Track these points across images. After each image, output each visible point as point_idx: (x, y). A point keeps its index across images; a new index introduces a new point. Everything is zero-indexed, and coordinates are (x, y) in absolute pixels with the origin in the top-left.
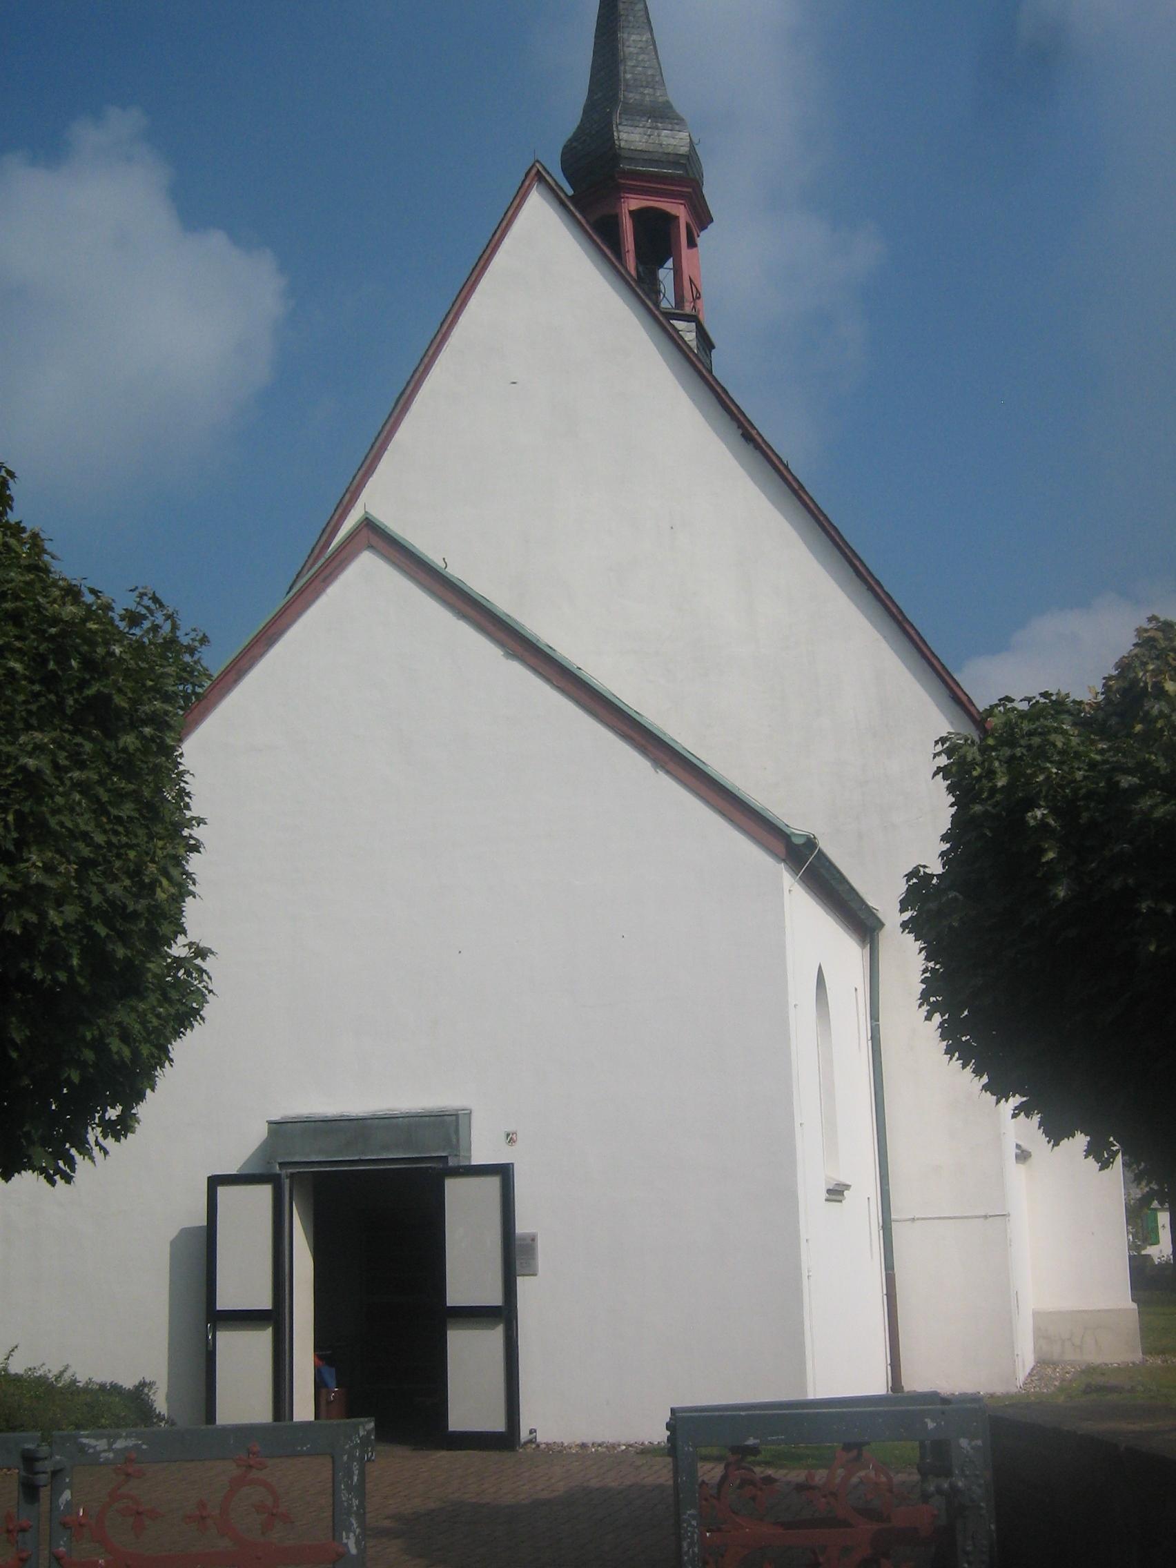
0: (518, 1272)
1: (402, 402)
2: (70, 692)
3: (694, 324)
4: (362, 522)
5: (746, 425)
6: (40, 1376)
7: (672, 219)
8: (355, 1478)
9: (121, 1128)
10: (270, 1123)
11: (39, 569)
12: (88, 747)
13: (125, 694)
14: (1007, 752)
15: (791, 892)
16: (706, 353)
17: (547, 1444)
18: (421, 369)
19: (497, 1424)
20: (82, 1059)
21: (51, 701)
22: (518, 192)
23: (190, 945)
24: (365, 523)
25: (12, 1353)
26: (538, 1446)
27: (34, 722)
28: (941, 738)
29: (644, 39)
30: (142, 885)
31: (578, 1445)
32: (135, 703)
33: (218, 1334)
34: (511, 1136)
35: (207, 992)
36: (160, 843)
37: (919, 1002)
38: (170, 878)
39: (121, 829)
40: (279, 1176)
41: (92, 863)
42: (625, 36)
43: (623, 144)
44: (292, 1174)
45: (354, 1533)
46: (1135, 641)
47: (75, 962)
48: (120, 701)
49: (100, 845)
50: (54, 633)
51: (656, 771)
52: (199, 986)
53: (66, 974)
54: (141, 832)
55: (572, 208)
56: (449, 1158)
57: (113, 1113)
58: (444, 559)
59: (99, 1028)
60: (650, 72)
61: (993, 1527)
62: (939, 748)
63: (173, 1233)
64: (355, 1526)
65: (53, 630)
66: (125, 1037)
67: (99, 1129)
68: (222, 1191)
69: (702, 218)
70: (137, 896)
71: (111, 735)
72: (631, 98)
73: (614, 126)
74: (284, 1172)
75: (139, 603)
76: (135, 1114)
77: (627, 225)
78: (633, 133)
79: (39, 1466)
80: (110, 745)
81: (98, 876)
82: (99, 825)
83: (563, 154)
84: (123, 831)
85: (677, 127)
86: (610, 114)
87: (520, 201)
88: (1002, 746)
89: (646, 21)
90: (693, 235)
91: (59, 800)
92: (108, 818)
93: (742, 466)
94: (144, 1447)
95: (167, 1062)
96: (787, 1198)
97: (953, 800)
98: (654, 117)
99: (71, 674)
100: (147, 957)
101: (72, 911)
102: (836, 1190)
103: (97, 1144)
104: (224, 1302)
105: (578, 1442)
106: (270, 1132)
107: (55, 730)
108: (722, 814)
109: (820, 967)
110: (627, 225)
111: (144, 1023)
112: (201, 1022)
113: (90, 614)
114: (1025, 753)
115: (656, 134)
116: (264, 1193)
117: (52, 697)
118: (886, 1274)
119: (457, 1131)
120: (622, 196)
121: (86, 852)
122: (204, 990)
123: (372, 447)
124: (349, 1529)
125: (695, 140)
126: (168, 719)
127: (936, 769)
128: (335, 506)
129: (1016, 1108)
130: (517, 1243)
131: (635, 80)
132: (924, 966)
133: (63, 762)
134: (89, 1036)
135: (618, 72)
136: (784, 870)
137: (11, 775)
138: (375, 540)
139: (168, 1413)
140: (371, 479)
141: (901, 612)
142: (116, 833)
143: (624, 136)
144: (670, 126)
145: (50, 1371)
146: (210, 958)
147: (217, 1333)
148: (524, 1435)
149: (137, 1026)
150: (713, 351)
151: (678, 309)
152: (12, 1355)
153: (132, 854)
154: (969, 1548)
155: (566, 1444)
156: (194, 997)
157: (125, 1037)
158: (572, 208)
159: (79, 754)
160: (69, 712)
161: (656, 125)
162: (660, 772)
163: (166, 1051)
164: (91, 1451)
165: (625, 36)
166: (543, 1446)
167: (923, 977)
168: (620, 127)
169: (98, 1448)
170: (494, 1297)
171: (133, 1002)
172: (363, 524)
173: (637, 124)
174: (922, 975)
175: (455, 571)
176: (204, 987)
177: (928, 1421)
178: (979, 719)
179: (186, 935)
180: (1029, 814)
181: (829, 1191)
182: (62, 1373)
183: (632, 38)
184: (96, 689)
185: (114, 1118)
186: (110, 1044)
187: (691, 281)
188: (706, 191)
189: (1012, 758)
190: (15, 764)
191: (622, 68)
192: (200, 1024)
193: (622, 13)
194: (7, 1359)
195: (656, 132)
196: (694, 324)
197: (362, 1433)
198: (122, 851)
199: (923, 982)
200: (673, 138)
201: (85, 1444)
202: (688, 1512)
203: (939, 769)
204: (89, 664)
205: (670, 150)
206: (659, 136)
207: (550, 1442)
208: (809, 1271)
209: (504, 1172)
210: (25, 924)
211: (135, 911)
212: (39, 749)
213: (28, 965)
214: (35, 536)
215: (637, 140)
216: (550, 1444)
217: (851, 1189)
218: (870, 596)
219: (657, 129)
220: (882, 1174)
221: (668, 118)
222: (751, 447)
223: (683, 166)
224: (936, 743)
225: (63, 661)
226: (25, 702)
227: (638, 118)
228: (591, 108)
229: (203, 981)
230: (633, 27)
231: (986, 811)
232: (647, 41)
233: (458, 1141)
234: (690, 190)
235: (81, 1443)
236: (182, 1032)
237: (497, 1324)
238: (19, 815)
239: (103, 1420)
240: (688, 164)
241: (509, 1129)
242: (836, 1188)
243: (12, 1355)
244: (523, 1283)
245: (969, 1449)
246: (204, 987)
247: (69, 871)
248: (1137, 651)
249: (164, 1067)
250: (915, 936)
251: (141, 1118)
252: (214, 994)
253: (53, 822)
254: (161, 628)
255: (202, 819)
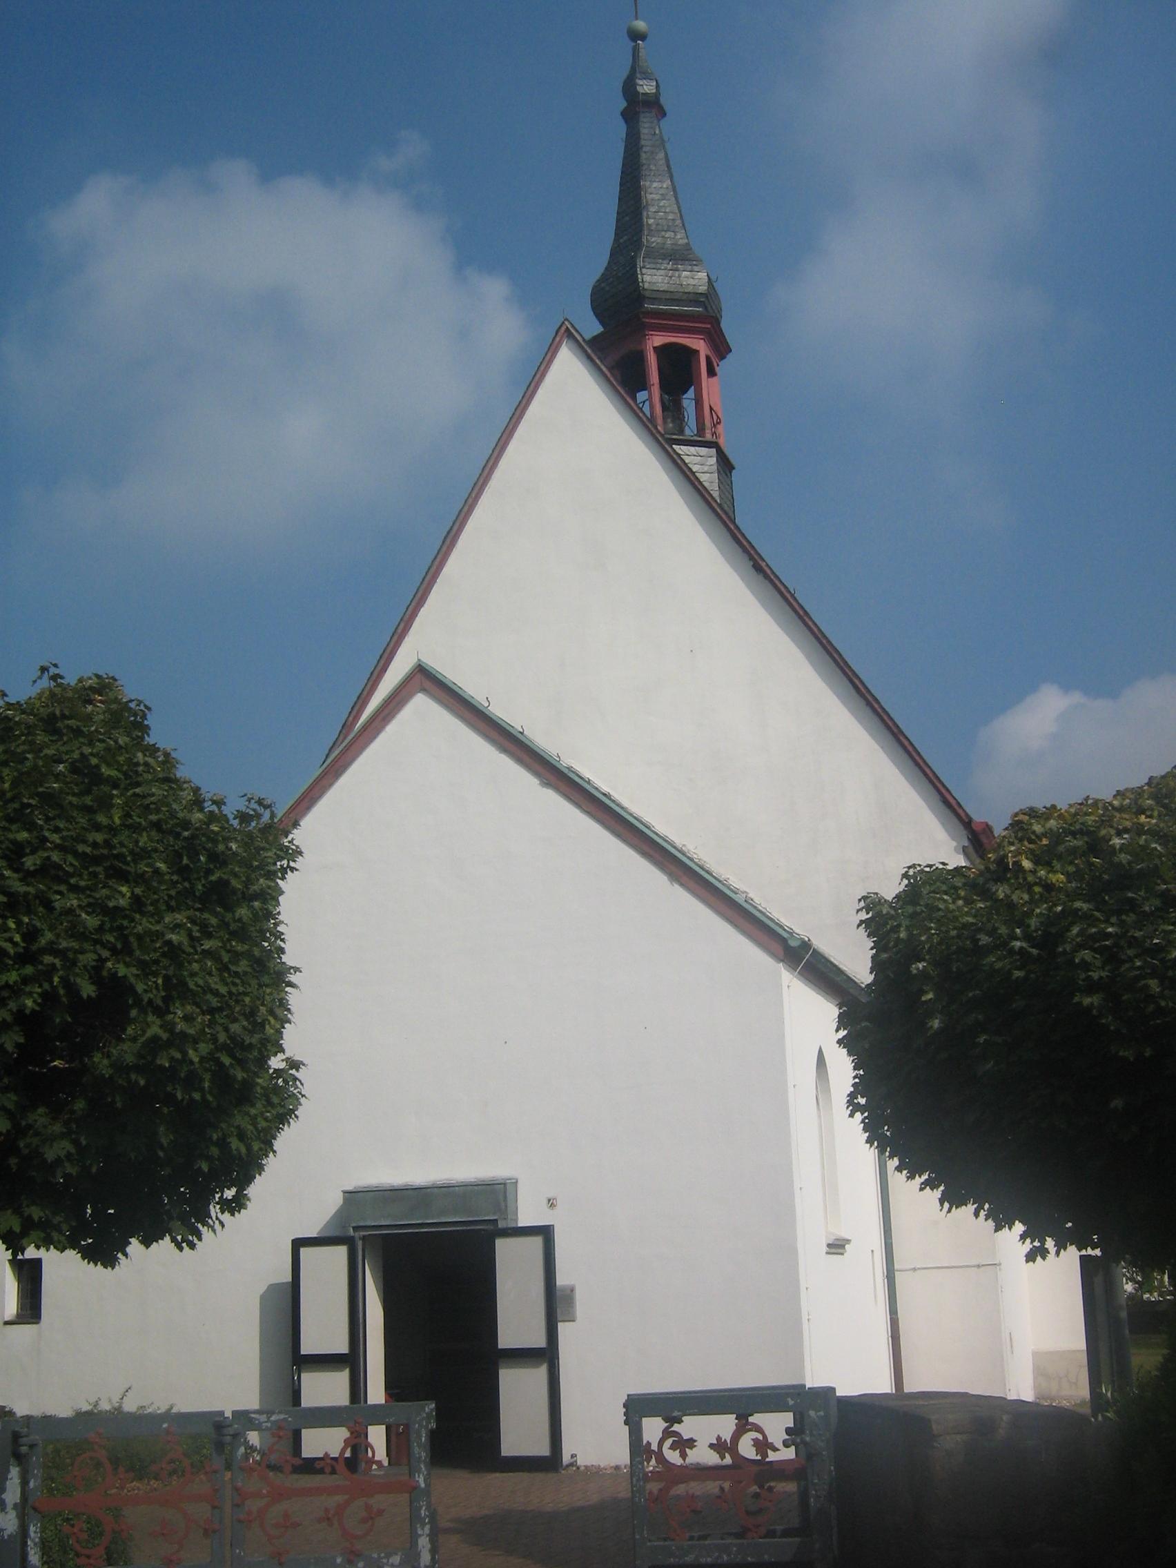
0: (559, 1319)
2: (199, 879)
3: (714, 450)
4: (416, 668)
8: (423, 1439)
9: (235, 1205)
10: (345, 1192)
11: (169, 780)
12: (214, 921)
13: (240, 877)
14: (910, 909)
16: (726, 475)
17: (586, 1467)
19: (544, 1450)
21: (186, 888)
23: (287, 1060)
25: (127, 1393)
26: (578, 1468)
27: (173, 903)
29: (665, 186)
30: (255, 1023)
31: (612, 1467)
32: (248, 882)
33: (303, 1375)
34: (551, 1201)
35: (300, 1096)
36: (268, 991)
37: (846, 1106)
38: (276, 1017)
39: (238, 981)
40: (353, 1237)
41: (220, 1009)
42: (648, 184)
43: (646, 286)
44: (364, 1236)
46: (1010, 822)
48: (235, 883)
51: (671, 883)
52: (295, 1091)
53: (199, 1094)
57: (230, 1193)
58: (487, 698)
59: (222, 1129)
61: (832, 1468)
62: (862, 904)
63: (262, 1288)
64: (423, 1469)
65: (186, 834)
66: (242, 1136)
67: (218, 1207)
68: (304, 1252)
69: (721, 348)
70: (251, 1032)
71: (229, 908)
72: (653, 242)
73: (638, 269)
77: (652, 360)
79: (226, 1431)
80: (229, 916)
82: (223, 980)
85: (696, 268)
86: (634, 259)
87: (547, 365)
90: (713, 366)
91: (196, 966)
92: (229, 974)
94: (290, 1419)
95: (271, 1153)
96: (787, 1253)
98: (674, 260)
100: (256, 1075)
101: (204, 1048)
102: (835, 1245)
103: (217, 1218)
104: (307, 1348)
105: (613, 1464)
106: (345, 1199)
109: (820, 1051)
110: (652, 360)
112: (296, 1119)
113: (212, 817)
114: (924, 909)
115: (677, 275)
116: (341, 1252)
117: (187, 884)
118: (891, 1319)
120: (647, 333)
121: (215, 1002)
122: (298, 1094)
123: (423, 580)
125: (713, 278)
129: (922, 1184)
130: (558, 1293)
131: (658, 225)
134: (215, 1137)
136: (783, 969)
137: (160, 948)
138: (428, 684)
142: (235, 984)
143: (647, 278)
146: (303, 1069)
147: (302, 1374)
148: (566, 1459)
150: (734, 471)
151: (700, 437)
152: (126, 1395)
153: (247, 1000)
154: (816, 1481)
155: (602, 1466)
157: (242, 1136)
162: (675, 884)
163: (271, 1145)
164: (257, 1422)
165: (648, 184)
167: (853, 1082)
168: (644, 271)
172: (417, 670)
174: (854, 1079)
175: (498, 710)
176: (298, 1092)
178: (967, 820)
179: (284, 1053)
180: (914, 966)
181: (829, 1246)
184: (218, 875)
185: (230, 1198)
187: (711, 409)
191: (645, 214)
192: (295, 1122)
193: (644, 162)
194: (122, 1398)
195: (677, 274)
196: (714, 450)
198: (240, 998)
200: (693, 278)
201: (253, 1418)
203: (862, 922)
204: (213, 857)
205: (690, 289)
206: (679, 276)
207: (589, 1464)
209: (546, 1233)
210: (172, 1059)
211: (251, 1044)
212: (177, 927)
214: (167, 755)
218: (868, 710)
220: (886, 1228)
222: (761, 577)
224: (860, 900)
229: (298, 1088)
230: (654, 175)
231: (890, 957)
232: (667, 188)
233: (506, 1206)
234: (709, 326)
235: (250, 1417)
236: (281, 1128)
237: (541, 1364)
238: (167, 979)
239: (205, 1451)
241: (550, 1196)
242: (835, 1243)
243: (126, 1395)
245: (815, 1417)
246: (298, 1092)
247: (205, 1021)
250: (848, 1050)
251: (251, 1197)
252: (306, 1098)
253: (192, 985)
254: (262, 815)
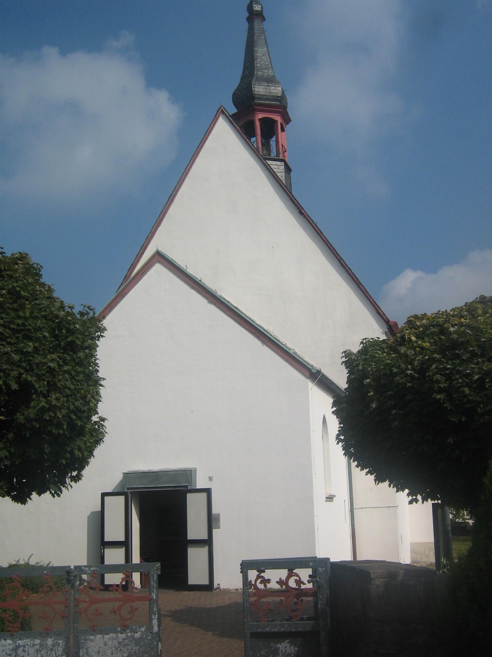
1: (171, 198)
2: (62, 340)
3: (283, 163)
5: (301, 208)
6: (41, 566)
7: (275, 122)
9: (77, 479)
10: (124, 473)
15: (312, 390)
18: (178, 186)
19: (206, 582)
20: (66, 457)
22: (214, 118)
23: (99, 417)
24: (157, 253)
25: (31, 557)
26: (221, 590)
27: (51, 350)
28: (344, 352)
30: (86, 402)
32: (83, 342)
35: (105, 433)
36: (92, 388)
37: (336, 439)
39: (79, 384)
41: (71, 395)
42: (257, 49)
44: (132, 492)
45: (155, 593)
47: (65, 427)
48: (78, 342)
49: (73, 389)
50: (57, 321)
54: (85, 384)
55: (235, 124)
56: (188, 486)
57: (74, 474)
59: (71, 446)
60: (267, 63)
61: (328, 592)
62: (343, 355)
63: (88, 514)
64: (155, 591)
66: (80, 449)
67: (70, 479)
69: (287, 120)
70: (84, 405)
71: (75, 352)
72: (259, 74)
73: (252, 85)
74: (129, 491)
75: (84, 310)
76: (81, 474)
77: (258, 124)
78: (260, 88)
79: (71, 574)
80: (75, 356)
81: (72, 399)
82: (72, 383)
83: (233, 96)
84: (79, 384)
85: (277, 86)
86: (251, 80)
88: (362, 355)
89: (265, 43)
93: (299, 224)
96: (310, 500)
97: (348, 372)
99: (63, 334)
100: (86, 423)
101: (64, 412)
103: (69, 484)
104: (107, 539)
105: (235, 588)
107: (58, 353)
108: (287, 361)
109: (324, 415)
110: (258, 124)
111: (85, 444)
112: (103, 442)
113: (68, 314)
116: (122, 498)
117: (57, 342)
119: (191, 476)
124: (153, 592)
125: (284, 90)
126: (93, 346)
127: (342, 362)
128: (146, 239)
129: (367, 472)
131: (261, 67)
132: (339, 426)
133: (61, 363)
134: (68, 449)
135: (254, 63)
136: (309, 382)
138: (161, 259)
139: (87, 579)
140: (159, 228)
141: (358, 280)
142: (77, 385)
143: (256, 89)
144: (274, 85)
145: (44, 563)
146: (106, 421)
147: (105, 550)
148: (215, 586)
149: (83, 446)
150: (291, 172)
152: (31, 558)
153: (83, 391)
156: (101, 434)
157: (80, 449)
158: (235, 124)
159: (65, 360)
160: (62, 346)
161: (269, 85)
162: (264, 346)
165: (257, 49)
166: (223, 590)
167: (338, 430)
169: (86, 570)
170: (205, 537)
171: (82, 438)
173: (261, 84)
175: (191, 271)
176: (104, 431)
177: (310, 563)
180: (365, 381)
181: (327, 498)
182: (49, 564)
183: (260, 50)
184: (71, 339)
185: (74, 475)
186: (75, 452)
188: (288, 110)
189: (365, 359)
190: (46, 365)
191: (256, 62)
194: (29, 559)
195: (269, 88)
196: (283, 163)
197: (157, 566)
198: (79, 391)
199: (338, 431)
200: (276, 90)
201: (83, 569)
202: (245, 588)
203: (343, 362)
204: (69, 331)
206: (270, 89)
207: (225, 588)
208: (318, 527)
209: (208, 491)
210: (50, 416)
212: (53, 360)
213: (51, 428)
214: (49, 287)
215: (262, 91)
216: (225, 589)
217: (336, 497)
219: (269, 86)
221: (274, 82)
222: (302, 216)
223: (280, 101)
224: (342, 353)
225: (60, 330)
226: (49, 344)
227: (262, 82)
228: (243, 78)
230: (260, 46)
233: (191, 480)
234: (282, 110)
235: (81, 569)
238: (48, 382)
240: (281, 99)
241: (210, 476)
243: (31, 558)
244: (215, 531)
246: (104, 431)
248: (404, 325)
249: (91, 458)
252: (107, 433)
255: (105, 378)
